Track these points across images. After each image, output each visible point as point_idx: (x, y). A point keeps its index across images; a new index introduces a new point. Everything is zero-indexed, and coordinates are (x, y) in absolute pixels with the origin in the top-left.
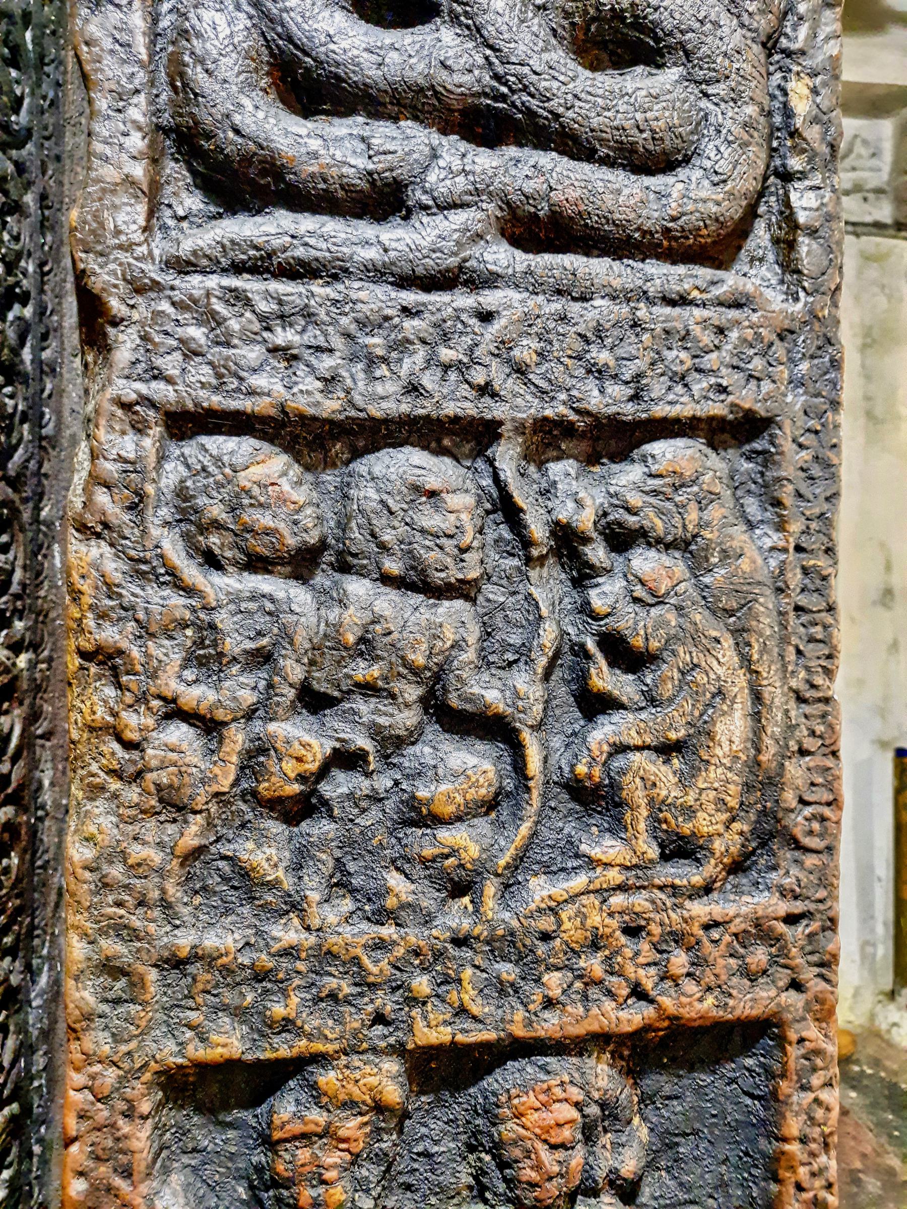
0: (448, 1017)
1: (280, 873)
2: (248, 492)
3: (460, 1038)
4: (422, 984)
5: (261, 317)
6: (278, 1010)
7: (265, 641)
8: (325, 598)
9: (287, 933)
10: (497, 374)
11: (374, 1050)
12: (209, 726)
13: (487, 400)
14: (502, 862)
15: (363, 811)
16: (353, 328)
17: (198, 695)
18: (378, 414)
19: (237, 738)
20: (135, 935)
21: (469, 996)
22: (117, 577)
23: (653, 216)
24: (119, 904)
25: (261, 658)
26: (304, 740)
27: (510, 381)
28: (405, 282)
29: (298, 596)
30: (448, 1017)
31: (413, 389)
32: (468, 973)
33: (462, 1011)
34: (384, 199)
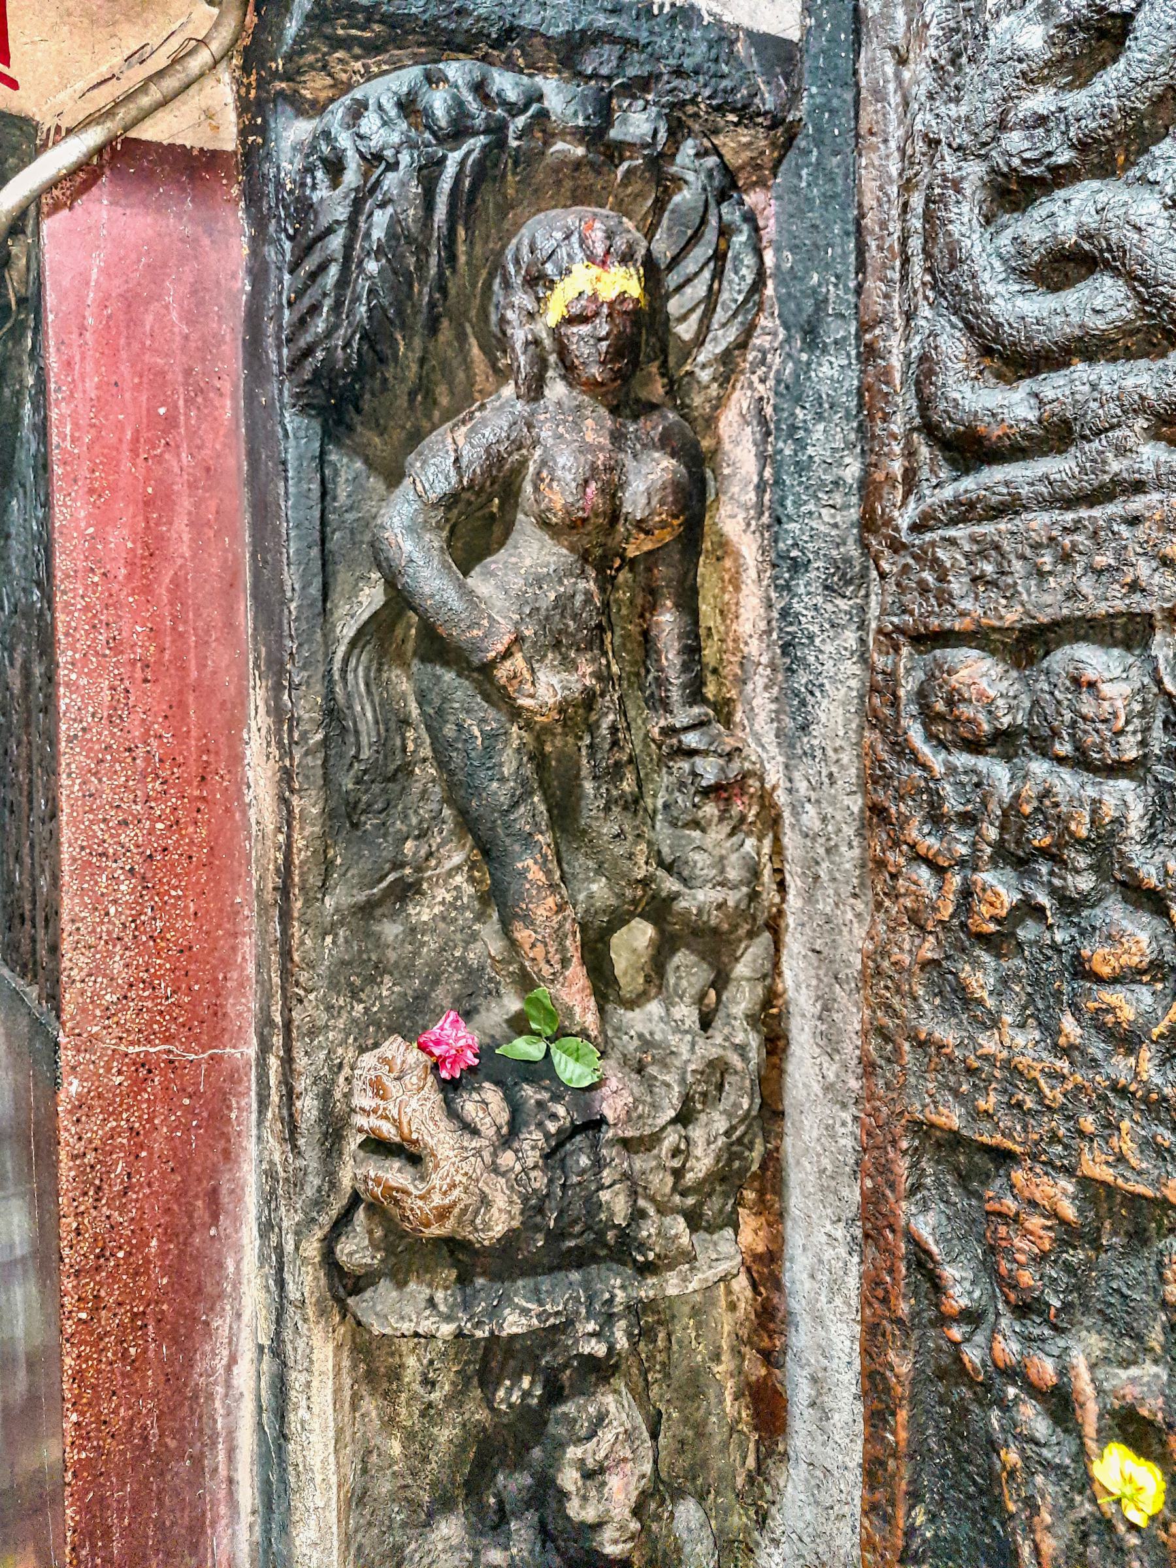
0: (1111, 1159)
1: (985, 995)
2: (958, 691)
3: (1120, 1181)
4: (1088, 1123)
5: (966, 556)
6: (982, 1104)
7: (970, 807)
8: (1020, 775)
9: (989, 1044)
10: (1144, 569)
11: (1050, 1163)
12: (939, 871)
13: (1137, 597)
14: (1156, 1031)
15: (1049, 958)
16: (1028, 552)
17: (931, 844)
18: (1046, 620)
19: (955, 880)
20: (896, 1014)
21: (1128, 1147)
22: (885, 756)
23: (1063, 328)
24: (887, 988)
25: (968, 820)
26: (1001, 889)
27: (1157, 575)
28: (1069, 503)
29: (998, 772)
30: (1111, 1159)
31: (1072, 594)
32: (1126, 1125)
33: (1121, 1159)
34: (1057, 434)
